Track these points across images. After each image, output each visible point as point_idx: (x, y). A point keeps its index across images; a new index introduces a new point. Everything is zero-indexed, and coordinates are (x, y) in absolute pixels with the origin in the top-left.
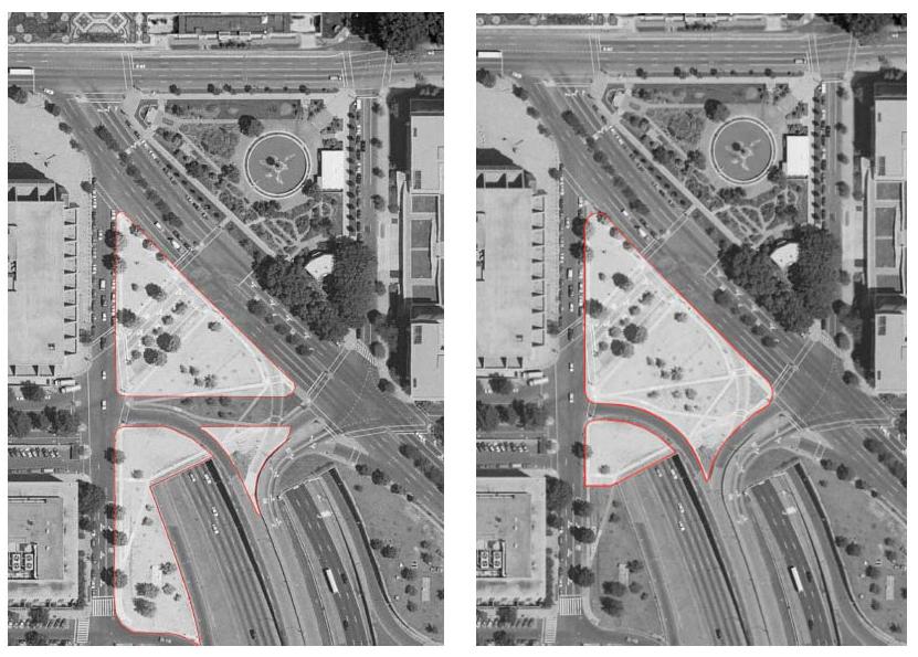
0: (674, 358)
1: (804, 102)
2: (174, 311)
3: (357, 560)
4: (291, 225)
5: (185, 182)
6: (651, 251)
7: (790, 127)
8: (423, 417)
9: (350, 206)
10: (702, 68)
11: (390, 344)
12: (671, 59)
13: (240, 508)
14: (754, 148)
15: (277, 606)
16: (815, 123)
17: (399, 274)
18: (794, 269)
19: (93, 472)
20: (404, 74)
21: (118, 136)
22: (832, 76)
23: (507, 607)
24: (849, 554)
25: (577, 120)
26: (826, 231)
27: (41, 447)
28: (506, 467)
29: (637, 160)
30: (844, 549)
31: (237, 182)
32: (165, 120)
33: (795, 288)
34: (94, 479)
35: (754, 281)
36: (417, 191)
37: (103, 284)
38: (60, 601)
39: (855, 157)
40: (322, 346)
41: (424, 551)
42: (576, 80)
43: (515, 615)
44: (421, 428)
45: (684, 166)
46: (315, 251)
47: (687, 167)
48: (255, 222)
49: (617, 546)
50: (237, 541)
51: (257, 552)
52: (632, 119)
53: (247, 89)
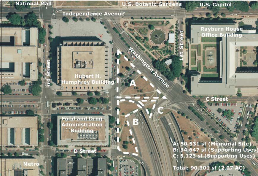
0: (141, 87)
1: (173, 25)
2: (132, 73)
3: (178, 135)
4: (161, 52)
5: (135, 41)
6: (135, 61)
7: (170, 31)
8: (194, 99)
9: (176, 47)
10: (148, 17)
11: (186, 81)
12: (140, 15)
13: (149, 122)
14: (161, 36)
15: (158, 147)
16: (176, 30)
17: (188, 64)
18: (171, 65)
19: (112, 113)
20: (189, 14)
21: (119, 30)
22: (180, 19)
23: (99, 147)
24: (184, 134)
25: (116, 30)
26: (179, 56)
27: (99, 107)
28: (99, 113)
29: (131, 39)
30: (183, 133)
31: (148, 41)
32: (130, 26)
33: (171, 70)
34: (112, 115)
35: (161, 68)
36: (192, 43)
37: (115, 67)
38: (92, 145)
39: (186, 39)
40: (169, 82)
41: (194, 133)
42: (116, 20)
43: (101, 148)
44: (194, 102)
45: (143, 41)
46: (167, 58)
47: (144, 41)
48: (152, 51)
49: (126, 132)
50: (148, 130)
51: (153, 133)
52: (130, 29)
53: (151, 18)
